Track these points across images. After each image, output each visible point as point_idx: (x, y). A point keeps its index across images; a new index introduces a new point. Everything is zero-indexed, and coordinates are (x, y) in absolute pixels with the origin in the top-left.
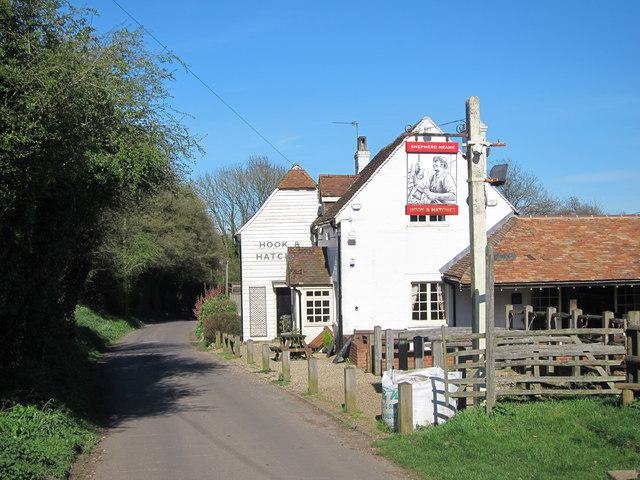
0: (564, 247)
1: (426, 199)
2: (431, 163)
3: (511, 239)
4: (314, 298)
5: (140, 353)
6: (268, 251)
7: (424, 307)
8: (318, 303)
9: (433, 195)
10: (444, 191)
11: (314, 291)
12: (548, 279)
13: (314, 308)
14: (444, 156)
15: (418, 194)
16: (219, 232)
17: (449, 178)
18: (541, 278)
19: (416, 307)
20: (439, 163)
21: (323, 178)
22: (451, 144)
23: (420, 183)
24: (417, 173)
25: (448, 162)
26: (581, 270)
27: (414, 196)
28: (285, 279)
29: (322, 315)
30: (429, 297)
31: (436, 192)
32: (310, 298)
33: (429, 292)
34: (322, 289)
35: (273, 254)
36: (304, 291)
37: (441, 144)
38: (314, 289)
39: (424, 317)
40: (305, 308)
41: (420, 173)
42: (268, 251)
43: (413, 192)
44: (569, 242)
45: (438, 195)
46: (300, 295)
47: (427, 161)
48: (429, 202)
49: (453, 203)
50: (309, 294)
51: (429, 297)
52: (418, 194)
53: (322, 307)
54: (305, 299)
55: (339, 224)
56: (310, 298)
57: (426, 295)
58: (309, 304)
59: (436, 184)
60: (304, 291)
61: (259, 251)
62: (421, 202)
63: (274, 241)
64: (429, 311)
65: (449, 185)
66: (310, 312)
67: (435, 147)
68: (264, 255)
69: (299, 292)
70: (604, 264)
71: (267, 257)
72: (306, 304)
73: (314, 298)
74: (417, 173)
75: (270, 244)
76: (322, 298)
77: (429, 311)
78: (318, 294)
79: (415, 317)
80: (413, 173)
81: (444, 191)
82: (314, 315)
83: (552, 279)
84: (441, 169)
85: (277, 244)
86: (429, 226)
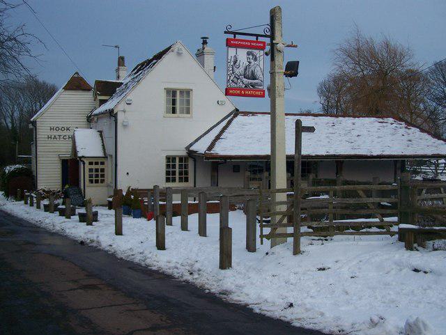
2: (245, 57)
4: (94, 167)
6: (56, 133)
7: (174, 173)
8: (97, 170)
10: (254, 78)
11: (94, 161)
13: (94, 173)
14: (256, 52)
16: (335, 71)
17: (258, 68)
19: (168, 173)
20: (251, 57)
21: (98, 83)
22: (261, 42)
23: (237, 71)
29: (94, 179)
30: (97, 167)
35: (60, 136)
37: (253, 42)
39: (174, 180)
41: (237, 64)
42: (56, 133)
43: (232, 78)
45: (250, 81)
46: (84, 163)
47: (242, 54)
51: (97, 167)
53: (100, 173)
55: (116, 114)
57: (175, 165)
58: (91, 170)
63: (60, 126)
65: (258, 73)
66: (91, 176)
71: (55, 137)
73: (94, 167)
75: (57, 129)
77: (177, 176)
79: (168, 180)
80: (232, 64)
81: (254, 78)
86: (179, 117)
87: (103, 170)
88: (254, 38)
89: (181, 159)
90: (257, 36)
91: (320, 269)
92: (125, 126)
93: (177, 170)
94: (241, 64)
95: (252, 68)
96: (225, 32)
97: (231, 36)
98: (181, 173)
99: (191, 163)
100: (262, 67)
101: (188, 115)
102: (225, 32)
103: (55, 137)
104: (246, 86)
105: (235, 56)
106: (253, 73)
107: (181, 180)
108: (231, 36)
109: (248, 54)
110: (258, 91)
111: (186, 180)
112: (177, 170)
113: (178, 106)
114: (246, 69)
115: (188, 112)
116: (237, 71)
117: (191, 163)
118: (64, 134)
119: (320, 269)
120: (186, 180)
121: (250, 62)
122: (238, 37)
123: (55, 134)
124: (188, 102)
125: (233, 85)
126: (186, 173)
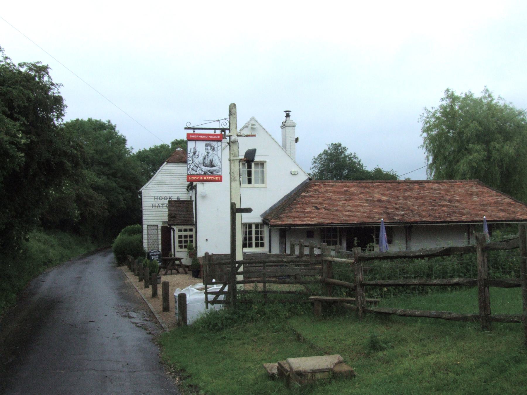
0: (339, 201)
1: (200, 171)
3: (305, 196)
4: (183, 233)
5: (250, 253)
7: (250, 239)
8: (186, 236)
9: (205, 169)
10: (212, 165)
11: (183, 228)
12: (326, 222)
13: (183, 239)
14: (214, 144)
15: (195, 168)
17: (216, 157)
18: (322, 221)
20: (209, 148)
23: (196, 161)
24: (194, 153)
25: (215, 147)
26: (349, 217)
27: (192, 169)
28: (167, 220)
31: (207, 166)
32: (181, 233)
33: (254, 230)
34: (188, 227)
35: (163, 204)
36: (176, 228)
38: (183, 227)
39: (250, 246)
40: (177, 239)
41: (197, 154)
43: (192, 167)
44: (343, 198)
45: (209, 168)
46: (174, 231)
48: (203, 173)
49: (219, 174)
50: (180, 230)
52: (195, 168)
53: (188, 239)
54: (177, 233)
56: (181, 233)
57: (252, 231)
58: (180, 237)
59: (207, 162)
60: (176, 228)
61: (155, 203)
62: (198, 173)
64: (254, 242)
65: (216, 161)
66: (180, 242)
67: (206, 137)
68: (157, 205)
69: (173, 229)
70: (364, 212)
71: (159, 206)
72: (178, 237)
73: (183, 233)
74: (194, 153)
76: (188, 233)
77: (254, 242)
78: (185, 230)
82: (183, 244)
83: (329, 222)
84: (211, 152)
85: (161, 198)
87: (191, 236)
88: (212, 132)
89: (257, 226)
90: (215, 129)
91: (105, 315)
92: (204, 197)
93: (254, 236)
94: (200, 154)
95: (211, 158)
96: (186, 128)
97: (191, 131)
98: (257, 239)
99: (266, 231)
100: (220, 156)
101: (263, 186)
102: (186, 128)
103: (159, 206)
104: (205, 173)
105: (195, 148)
106: (211, 162)
107: (257, 245)
108: (191, 131)
109: (207, 145)
110: (216, 177)
111: (262, 245)
112: (254, 236)
113: (253, 177)
114: (204, 159)
115: (263, 182)
116: (196, 161)
117: (266, 231)
118: (162, 202)
119: (105, 315)
120: (262, 245)
121: (208, 153)
122: (197, 132)
123: (159, 203)
124: (263, 173)
125: (193, 173)
126: (262, 239)
